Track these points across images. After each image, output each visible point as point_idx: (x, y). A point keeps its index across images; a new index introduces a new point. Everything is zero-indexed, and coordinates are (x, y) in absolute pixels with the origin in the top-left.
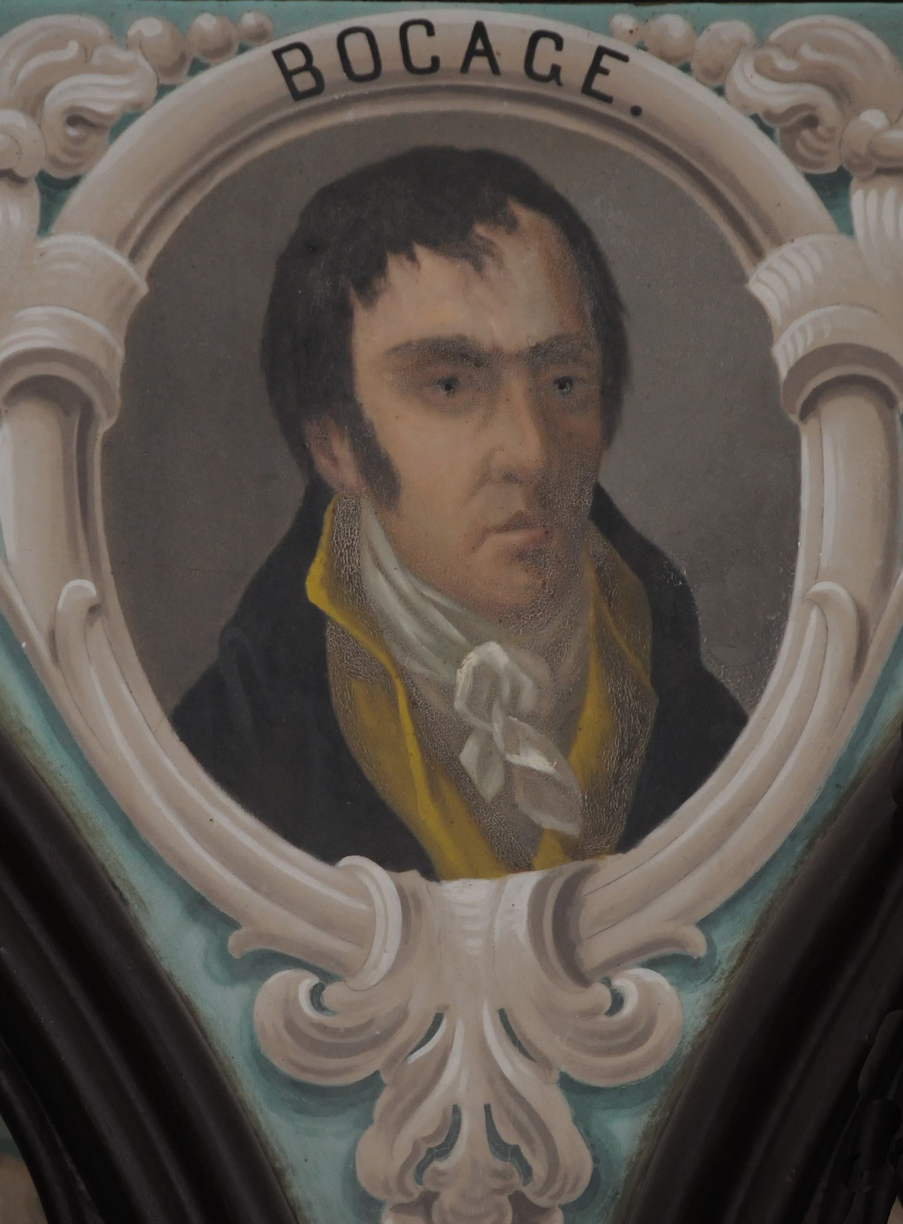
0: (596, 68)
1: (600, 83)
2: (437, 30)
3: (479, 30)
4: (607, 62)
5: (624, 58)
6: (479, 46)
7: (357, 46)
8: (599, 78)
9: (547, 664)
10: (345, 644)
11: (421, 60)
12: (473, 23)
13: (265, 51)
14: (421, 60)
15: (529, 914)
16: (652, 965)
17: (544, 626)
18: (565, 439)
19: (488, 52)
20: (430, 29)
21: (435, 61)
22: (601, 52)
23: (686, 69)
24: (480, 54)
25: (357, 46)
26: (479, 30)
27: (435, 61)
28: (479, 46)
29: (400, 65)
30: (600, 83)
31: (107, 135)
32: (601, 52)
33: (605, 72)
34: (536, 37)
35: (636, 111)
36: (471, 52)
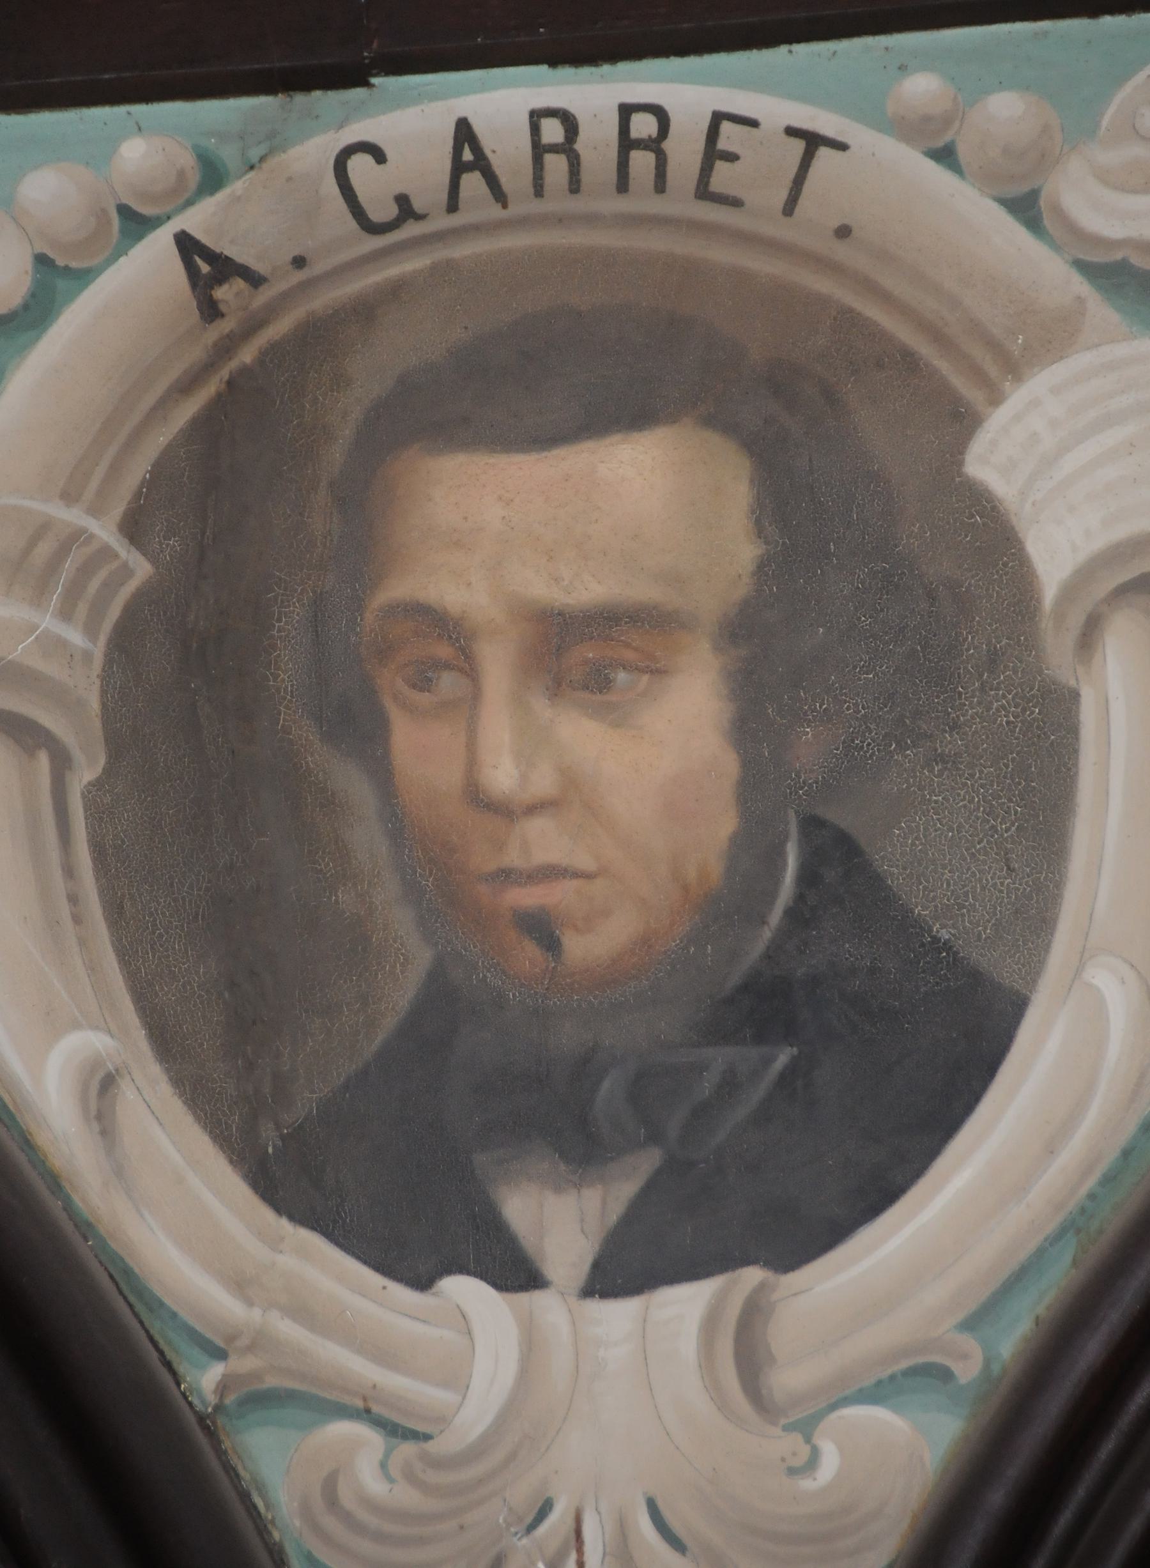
0: (713, 153)
3: (464, 132)
6: (467, 155)
8: (720, 166)
9: (606, 958)
11: (381, 210)
12: (510, 206)
13: (161, 241)
14: (381, 210)
15: (964, 1123)
16: (874, 1395)
19: (482, 164)
20: (379, 155)
21: (402, 200)
22: (718, 118)
23: (945, 156)
24: (469, 167)
26: (464, 132)
27: (402, 200)
28: (467, 155)
30: (723, 177)
32: (718, 118)
33: (731, 157)
35: (299, 262)
36: (459, 168)
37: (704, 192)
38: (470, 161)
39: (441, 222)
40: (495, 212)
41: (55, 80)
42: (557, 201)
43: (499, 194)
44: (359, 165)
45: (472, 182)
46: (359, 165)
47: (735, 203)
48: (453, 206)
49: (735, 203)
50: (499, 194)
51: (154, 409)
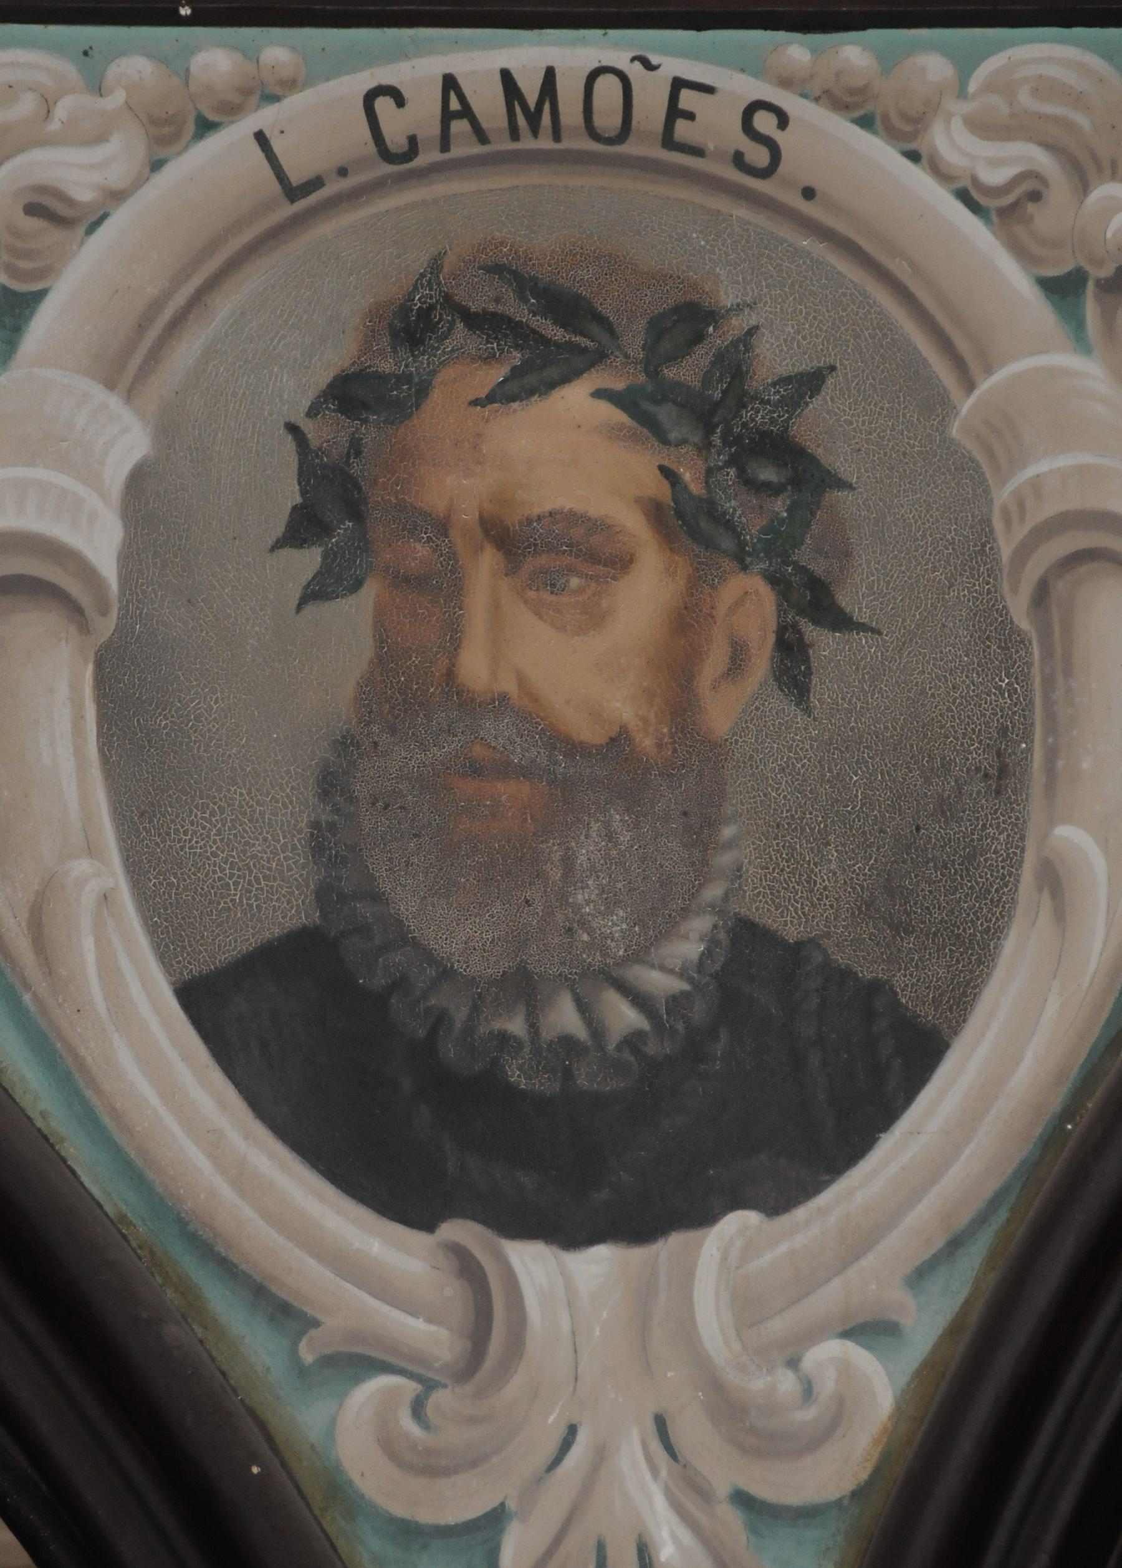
0: (674, 112)
1: (296, 177)
2: (407, 94)
3: (450, 83)
4: (688, 99)
5: (709, 90)
6: (455, 105)
7: (608, 90)
10: (783, 888)
15: (535, 1241)
17: (252, 878)
18: (620, 754)
19: (466, 112)
20: (397, 96)
24: (458, 115)
25: (608, 90)
26: (450, 83)
28: (455, 105)
29: (578, 119)
31: (81, 229)
33: (690, 116)
34: (370, 98)
35: (809, 193)
36: (447, 116)
37: (668, 140)
38: (459, 111)
39: (436, 156)
40: (478, 149)
41: (316, 7)
42: (464, 147)
43: (481, 136)
44: (383, 105)
45: (460, 126)
46: (383, 105)
47: (698, 152)
48: (445, 146)
49: (698, 152)
50: (481, 136)
51: (141, 369)
